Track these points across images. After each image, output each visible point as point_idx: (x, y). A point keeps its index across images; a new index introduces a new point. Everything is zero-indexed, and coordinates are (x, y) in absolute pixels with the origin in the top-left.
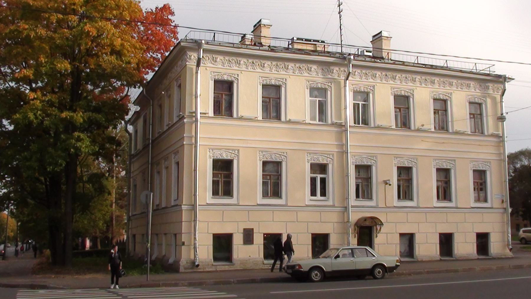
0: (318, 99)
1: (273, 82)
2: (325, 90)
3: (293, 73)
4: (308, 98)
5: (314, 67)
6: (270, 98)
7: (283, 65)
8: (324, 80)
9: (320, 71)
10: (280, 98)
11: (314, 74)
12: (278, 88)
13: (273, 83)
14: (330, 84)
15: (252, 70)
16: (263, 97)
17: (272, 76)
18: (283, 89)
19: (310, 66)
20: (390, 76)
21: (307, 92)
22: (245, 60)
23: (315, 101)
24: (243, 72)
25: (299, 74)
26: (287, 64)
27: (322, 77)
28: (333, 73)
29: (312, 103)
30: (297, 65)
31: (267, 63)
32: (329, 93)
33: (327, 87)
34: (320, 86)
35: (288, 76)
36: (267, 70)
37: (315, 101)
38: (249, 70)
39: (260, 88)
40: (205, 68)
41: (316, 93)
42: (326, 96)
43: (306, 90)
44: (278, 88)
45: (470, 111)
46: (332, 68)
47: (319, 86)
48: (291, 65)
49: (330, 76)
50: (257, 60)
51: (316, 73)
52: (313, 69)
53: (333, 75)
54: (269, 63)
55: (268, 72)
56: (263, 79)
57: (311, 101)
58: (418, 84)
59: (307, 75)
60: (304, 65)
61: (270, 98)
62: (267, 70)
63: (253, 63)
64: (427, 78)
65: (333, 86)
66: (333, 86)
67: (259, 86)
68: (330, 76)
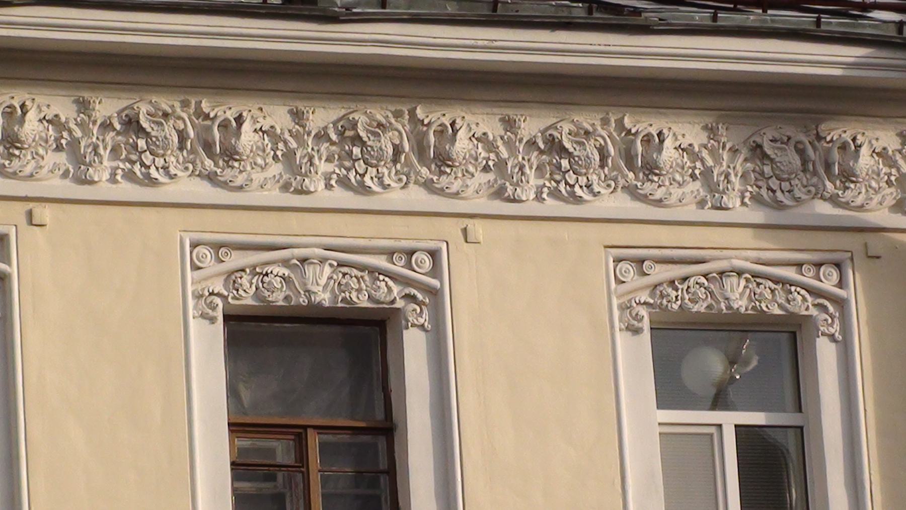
0: (730, 419)
1: (321, 289)
2: (787, 339)
3: (499, 194)
4: (644, 419)
5: (681, 133)
6: (299, 434)
7: (403, 126)
8: (772, 249)
9: (734, 169)
10: (387, 430)
11: (683, 196)
12: (359, 341)
13: (324, 298)
14: (828, 282)
15: (126, 190)
16: (235, 428)
17: (307, 232)
18: (414, 347)
19: (643, 124)
20: (170, 132)
21: (635, 356)
22: (61, 105)
23: (709, 439)
24: (44, 213)
25: (552, 207)
26: (435, 116)
27: (758, 216)
28: (848, 176)
29: (684, 458)
30: (532, 124)
31: (262, 119)
32: (826, 354)
33: (803, 305)
34: (741, 304)
35: (452, 228)
36: (262, 181)
37: (709, 439)
38: (104, 190)
39: (208, 345)
40: (21, 208)
41: (712, 364)
42: (798, 391)
43: (621, 338)
44: (359, 341)
45: (229, 419)
46: (839, 131)
47: (738, 297)
48: (473, 126)
49: (824, 208)
50: (165, 102)
51: (695, 187)
52: (668, 154)
53: (855, 194)
54: (277, 115)
55: (691, 212)
56: (236, 260)
57: (670, 439)
58: (474, 189)
59: (203, 191)
60: (588, 119)
61: (299, 434)
62: (262, 181)
63: (132, 124)
64: (565, 134)
65: (856, 293)
66: (856, 293)
67: (194, 325)
68: (824, 208)
